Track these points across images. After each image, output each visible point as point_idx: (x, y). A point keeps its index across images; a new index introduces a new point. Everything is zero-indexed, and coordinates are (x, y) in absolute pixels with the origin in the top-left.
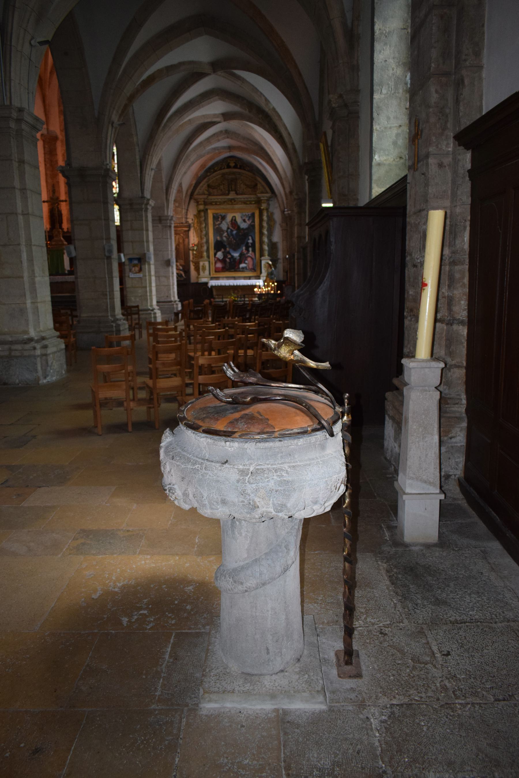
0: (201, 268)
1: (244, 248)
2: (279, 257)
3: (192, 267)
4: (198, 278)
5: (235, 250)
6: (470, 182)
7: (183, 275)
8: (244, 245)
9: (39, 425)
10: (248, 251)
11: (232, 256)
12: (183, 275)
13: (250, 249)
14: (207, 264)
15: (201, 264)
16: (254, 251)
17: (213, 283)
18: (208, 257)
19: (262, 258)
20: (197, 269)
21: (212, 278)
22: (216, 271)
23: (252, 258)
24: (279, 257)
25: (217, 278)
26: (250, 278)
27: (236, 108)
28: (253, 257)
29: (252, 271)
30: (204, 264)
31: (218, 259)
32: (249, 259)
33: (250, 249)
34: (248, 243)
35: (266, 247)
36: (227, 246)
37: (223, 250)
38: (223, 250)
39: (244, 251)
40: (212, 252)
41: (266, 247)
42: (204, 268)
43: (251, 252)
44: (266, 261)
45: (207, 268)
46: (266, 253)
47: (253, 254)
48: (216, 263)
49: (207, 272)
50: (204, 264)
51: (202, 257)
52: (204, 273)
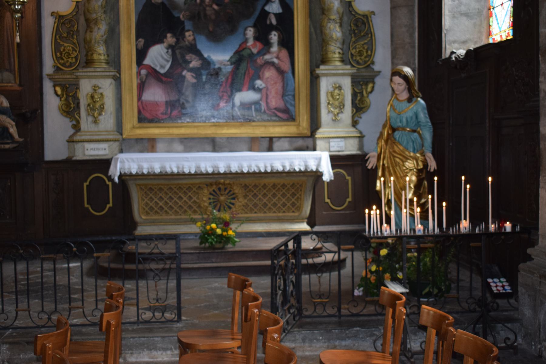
0: (84, 102)
1: (250, 32)
2: (376, 68)
3: (52, 102)
4: (71, 141)
5: (216, 38)
6: (210, 170)
7: (13, 130)
8: (252, 21)
9: (502, 5)
10: (267, 44)
11: (206, 63)
12: (13, 130)
13: (274, 37)
14: (107, 87)
15: (85, 87)
16: (288, 43)
17: (129, 163)
18: (114, 62)
19: (322, 69)
20: (70, 109)
21: (127, 145)
22: (141, 119)
23: (281, 72)
24: (376, 68)
25: (149, 145)
26: (270, 144)
27: (361, 313)
28: (286, 66)
29: (282, 120)
30: (95, 88)
31: (153, 73)
32: (269, 73)
33: (274, 37)
34: (265, 14)
35: (335, 32)
36: (188, 25)
37: (170, 39)
38: (170, 39)
39: (251, 43)
40: (128, 47)
41: (335, 32)
42: (96, 107)
43: (275, 48)
44: (335, 81)
45: (109, 103)
46: (335, 51)
47: (284, 53)
48: (141, 87)
49: (107, 121)
50: (95, 88)
51: (89, 62)
52: (96, 121)
